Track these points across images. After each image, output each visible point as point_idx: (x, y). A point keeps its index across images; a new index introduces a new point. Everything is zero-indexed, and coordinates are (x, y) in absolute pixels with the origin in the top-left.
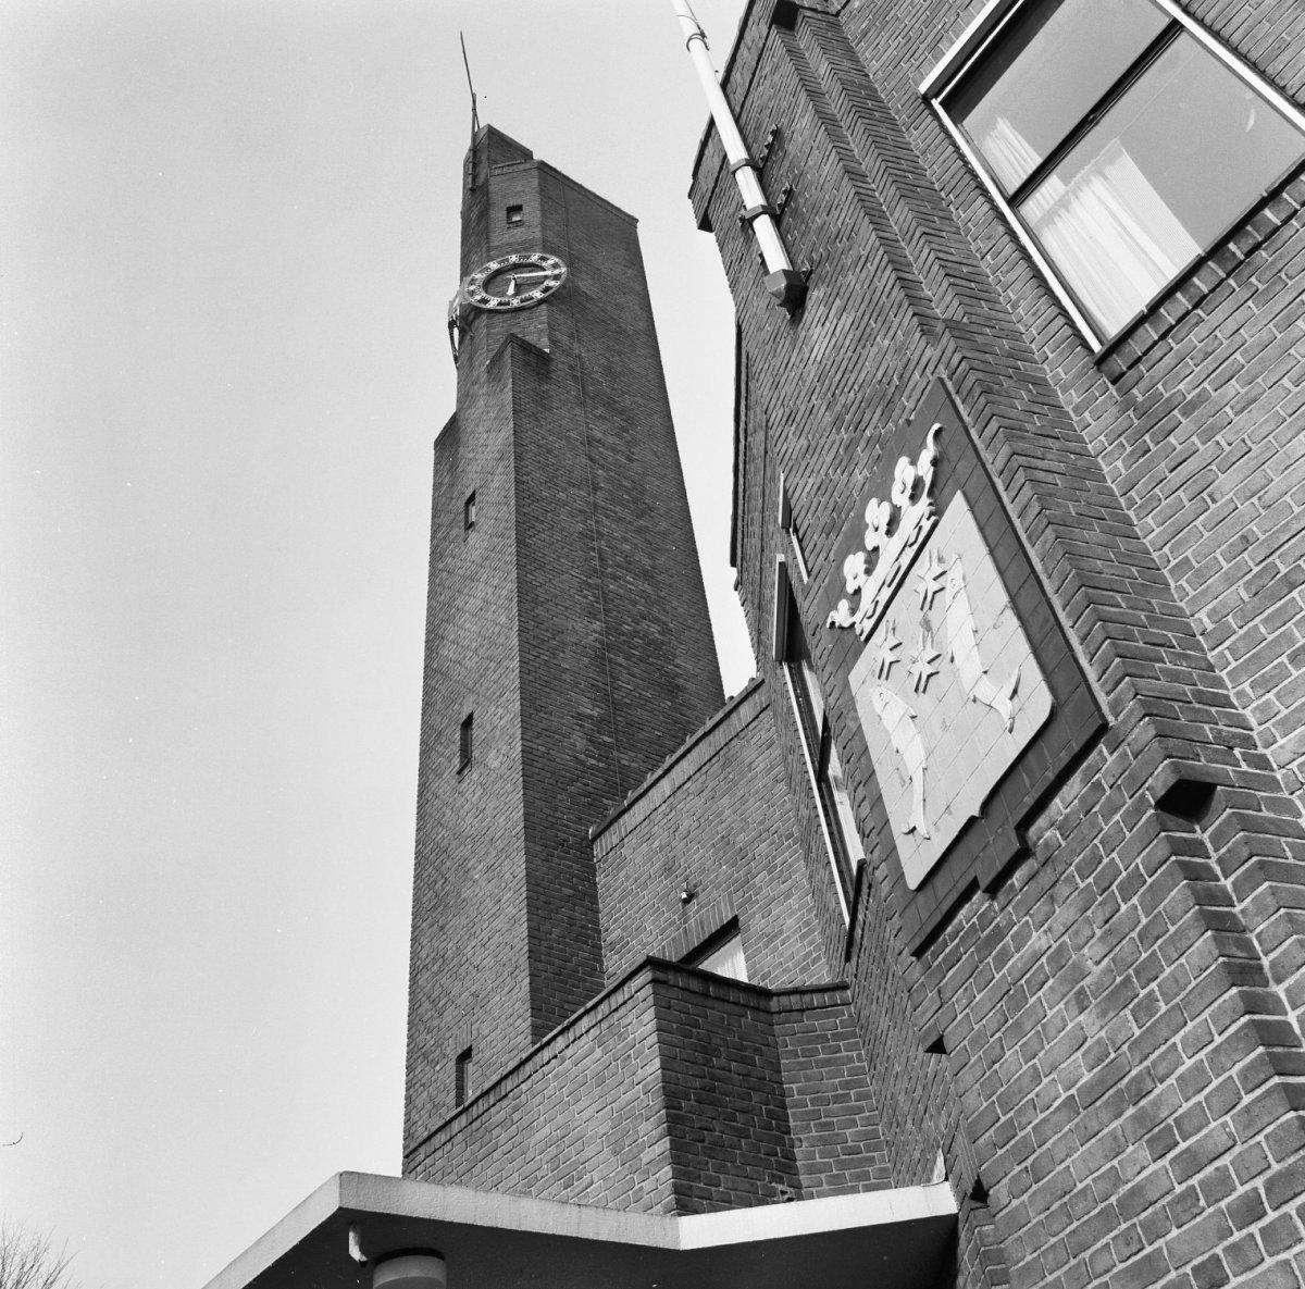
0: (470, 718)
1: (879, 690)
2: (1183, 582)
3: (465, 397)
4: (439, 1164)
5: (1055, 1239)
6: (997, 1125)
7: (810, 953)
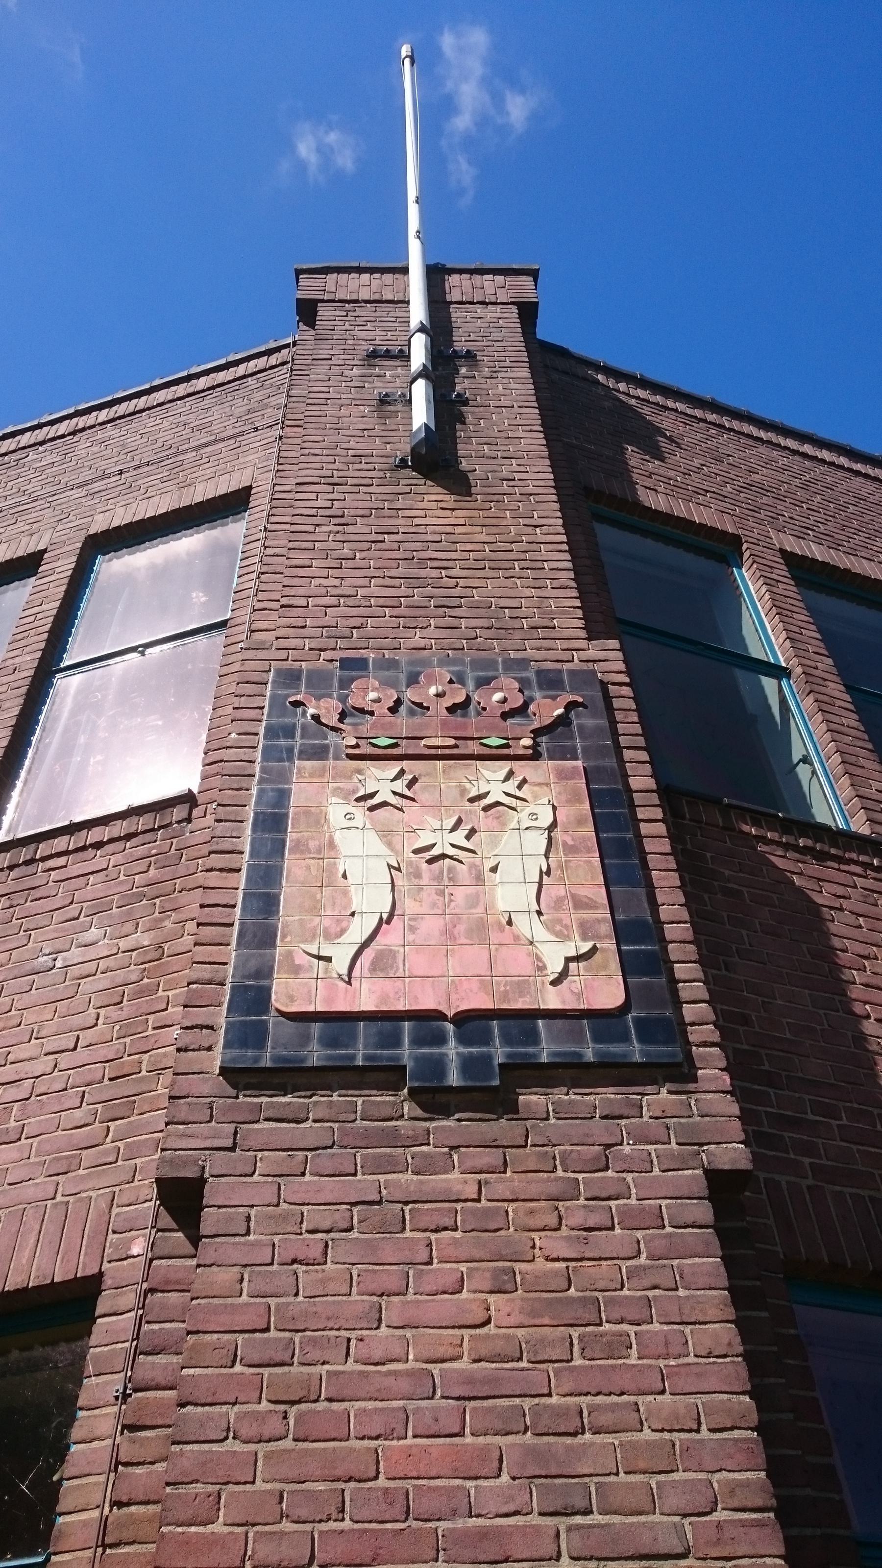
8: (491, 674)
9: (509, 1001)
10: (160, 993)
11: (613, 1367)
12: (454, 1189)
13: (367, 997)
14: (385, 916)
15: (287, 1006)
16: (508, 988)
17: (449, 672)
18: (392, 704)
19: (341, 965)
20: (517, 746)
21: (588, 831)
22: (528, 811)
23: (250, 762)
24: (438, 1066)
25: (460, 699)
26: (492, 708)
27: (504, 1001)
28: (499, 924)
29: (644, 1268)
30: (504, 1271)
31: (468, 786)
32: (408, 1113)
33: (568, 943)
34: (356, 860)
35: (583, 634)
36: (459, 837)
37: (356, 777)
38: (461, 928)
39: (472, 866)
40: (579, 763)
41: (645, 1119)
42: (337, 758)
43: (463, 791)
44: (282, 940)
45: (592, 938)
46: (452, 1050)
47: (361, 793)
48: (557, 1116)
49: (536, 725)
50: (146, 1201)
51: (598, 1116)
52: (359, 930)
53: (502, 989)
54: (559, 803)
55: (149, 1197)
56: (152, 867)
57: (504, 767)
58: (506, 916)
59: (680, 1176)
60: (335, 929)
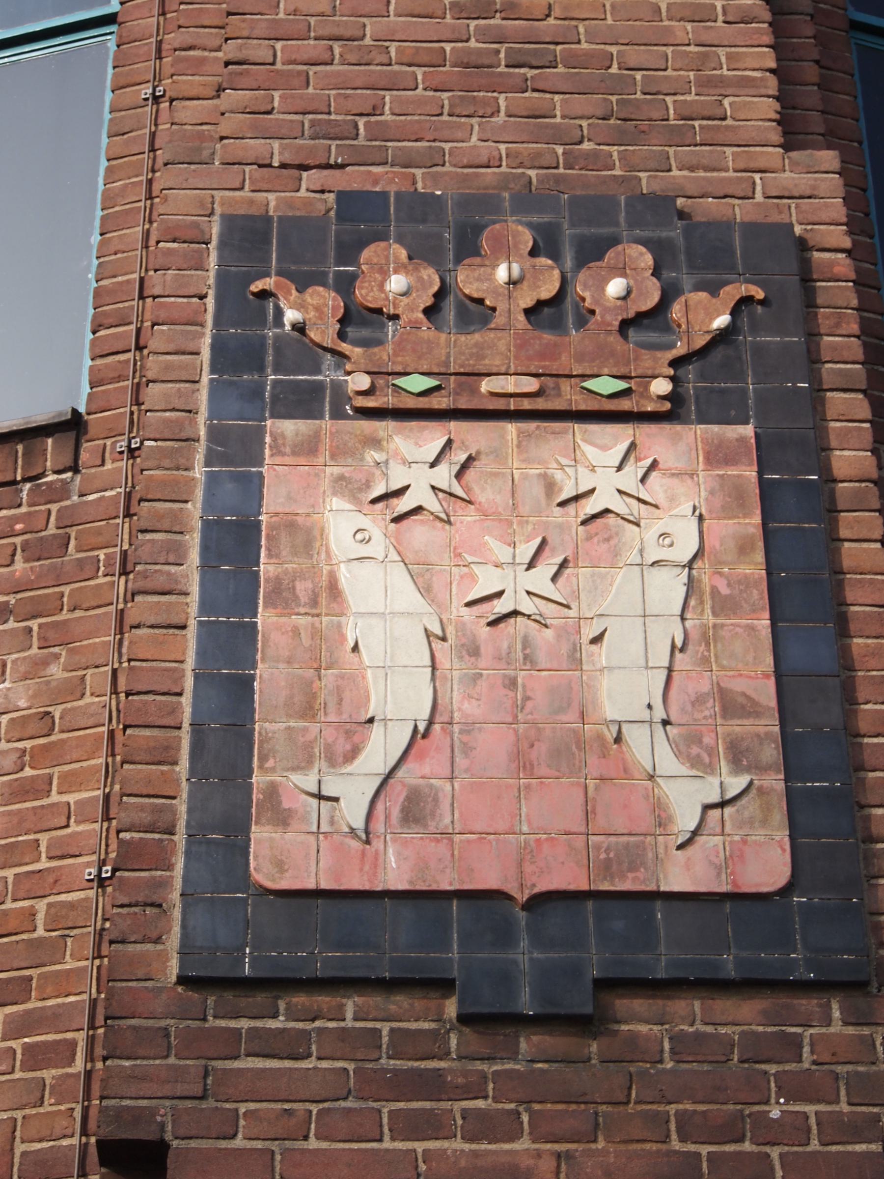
8: (605, 231)
9: (612, 877)
10: (55, 797)
12: (523, 1166)
13: (395, 871)
14: (422, 727)
15: (273, 880)
16: (612, 855)
17: (530, 226)
18: (429, 301)
19: (353, 812)
20: (645, 393)
21: (754, 568)
22: (659, 527)
23: (190, 411)
24: (505, 978)
25: (548, 290)
26: (606, 310)
27: (605, 878)
28: (600, 737)
31: (558, 475)
32: (458, 1049)
33: (710, 779)
34: (374, 621)
35: (775, 136)
37: (373, 455)
38: (542, 749)
39: (562, 633)
40: (748, 431)
42: (338, 414)
43: (550, 487)
44: (261, 767)
45: (748, 770)
46: (524, 955)
47: (379, 490)
48: (677, 1057)
49: (681, 349)
50: (65, 1137)
51: (736, 1059)
52: (380, 750)
53: (603, 856)
54: (710, 511)
55: (69, 1131)
56: (18, 557)
57: (620, 436)
58: (614, 729)
59: (849, 1152)
60: (342, 746)
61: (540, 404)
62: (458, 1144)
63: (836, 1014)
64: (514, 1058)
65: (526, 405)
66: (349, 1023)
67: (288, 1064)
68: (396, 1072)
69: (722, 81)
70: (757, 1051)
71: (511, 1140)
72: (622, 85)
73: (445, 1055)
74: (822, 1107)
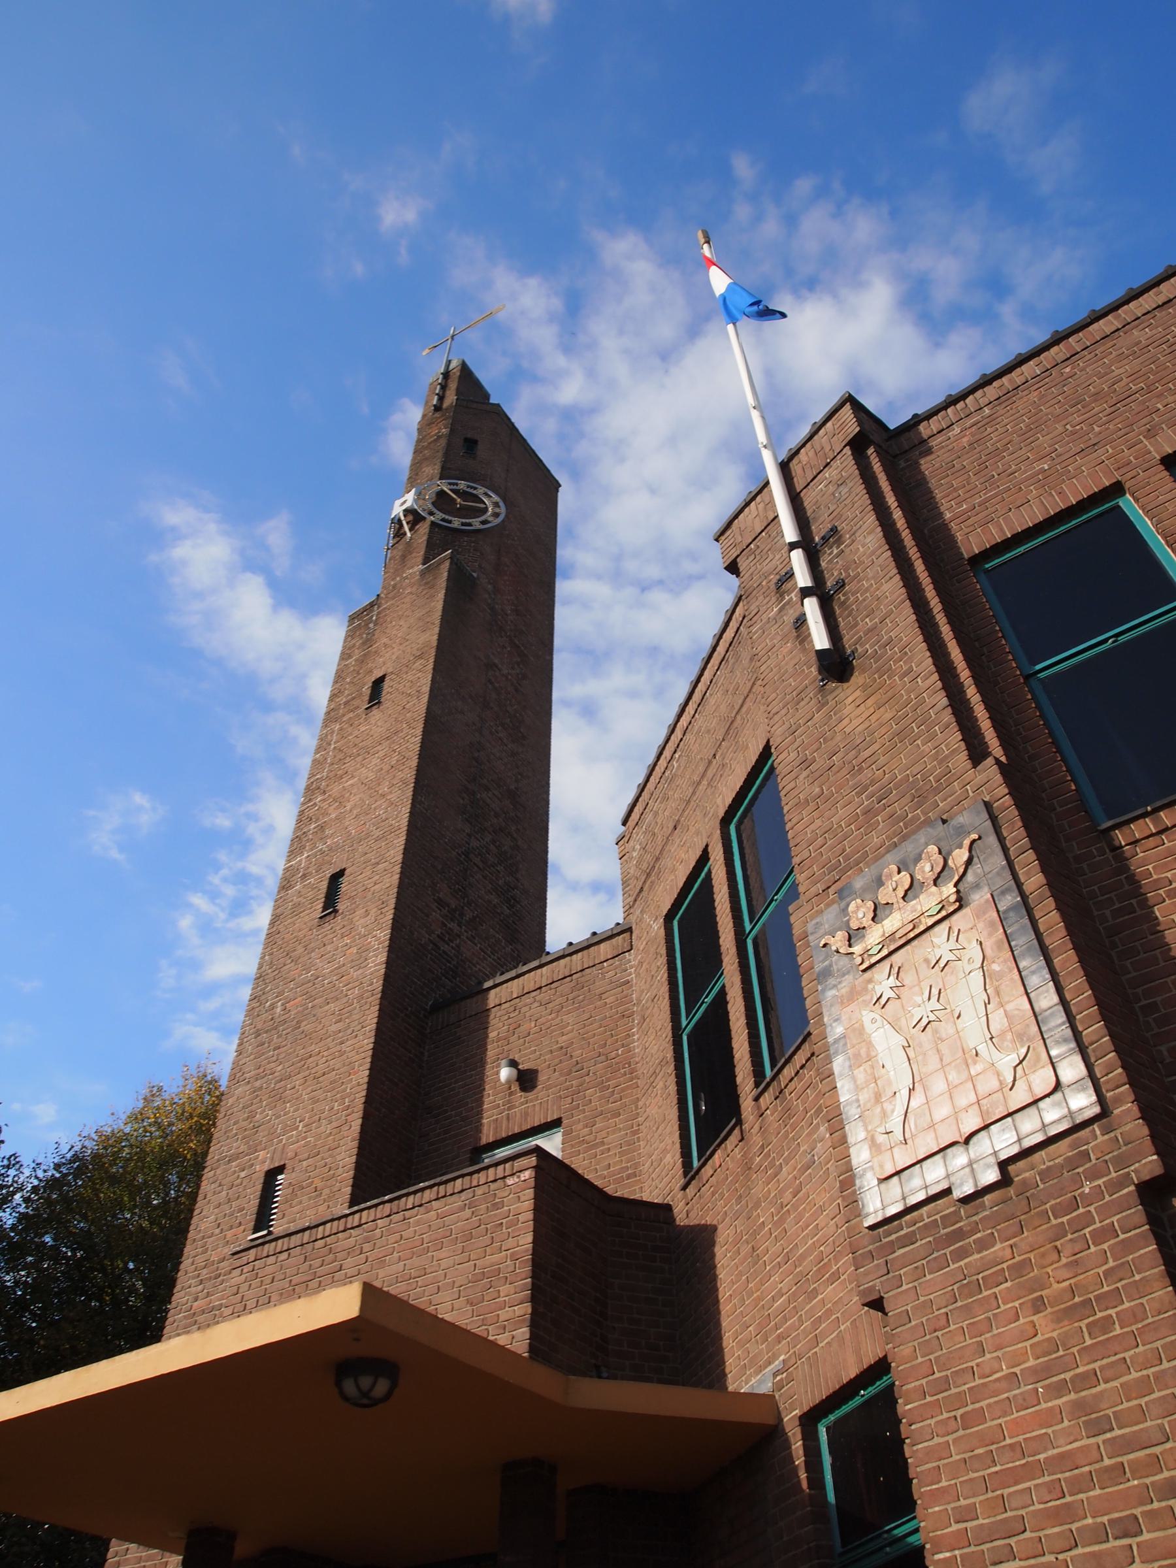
0: (341, 873)
1: (872, 1015)
2: (1150, 1019)
3: (392, 590)
4: (269, 1269)
5: (976, 1475)
6: (931, 1378)
7: (627, 1168)
11: (1108, 1339)
18: (872, 915)
29: (1112, 1269)
30: (1037, 1299)
36: (934, 1005)
41: (1094, 1161)
43: (927, 961)
61: (917, 931)
62: (976, 1256)
63: (1098, 1132)
64: (985, 1210)
65: (912, 935)
66: (927, 1221)
67: (912, 1247)
68: (946, 1234)
69: (946, 757)
70: (1072, 1164)
71: (993, 1246)
72: (916, 781)
73: (961, 1220)
74: (1105, 1179)
